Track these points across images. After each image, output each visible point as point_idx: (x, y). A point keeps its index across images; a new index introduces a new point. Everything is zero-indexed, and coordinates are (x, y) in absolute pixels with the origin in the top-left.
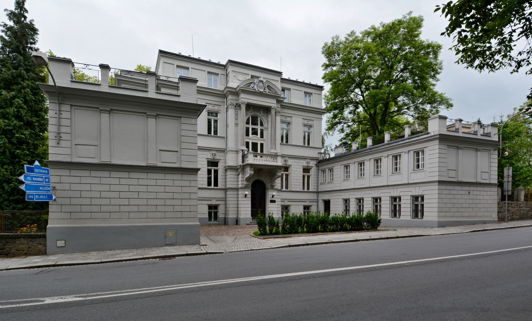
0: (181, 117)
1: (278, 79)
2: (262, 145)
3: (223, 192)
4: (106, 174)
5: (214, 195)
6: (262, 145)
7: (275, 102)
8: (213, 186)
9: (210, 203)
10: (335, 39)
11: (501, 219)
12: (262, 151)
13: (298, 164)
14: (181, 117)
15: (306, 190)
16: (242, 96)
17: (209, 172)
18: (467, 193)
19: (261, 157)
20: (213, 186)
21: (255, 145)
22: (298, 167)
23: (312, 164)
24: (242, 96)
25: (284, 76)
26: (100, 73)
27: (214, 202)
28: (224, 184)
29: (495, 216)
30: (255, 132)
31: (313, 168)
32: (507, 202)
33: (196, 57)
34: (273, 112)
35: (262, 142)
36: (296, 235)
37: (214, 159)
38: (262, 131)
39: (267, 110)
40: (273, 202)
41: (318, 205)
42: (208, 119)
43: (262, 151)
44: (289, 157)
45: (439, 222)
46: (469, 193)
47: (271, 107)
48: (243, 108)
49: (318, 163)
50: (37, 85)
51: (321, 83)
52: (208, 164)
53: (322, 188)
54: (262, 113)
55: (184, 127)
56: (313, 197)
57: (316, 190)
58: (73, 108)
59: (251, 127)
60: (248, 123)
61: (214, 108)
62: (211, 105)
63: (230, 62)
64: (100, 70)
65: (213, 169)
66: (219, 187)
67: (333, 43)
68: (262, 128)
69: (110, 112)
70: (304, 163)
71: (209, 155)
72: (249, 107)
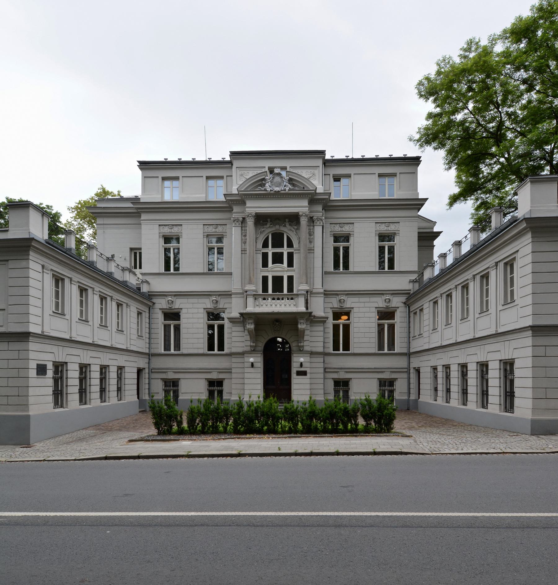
1: (320, 162)
2: (290, 278)
3: (405, 359)
5: (215, 363)
6: (290, 278)
7: (305, 203)
8: (216, 351)
9: (209, 376)
10: (442, 65)
12: (290, 289)
13: (367, 305)
16: (249, 203)
19: (264, 299)
20: (172, 351)
21: (278, 281)
22: (196, 311)
23: (397, 302)
24: (249, 203)
25: (328, 157)
27: (214, 376)
28: (405, 345)
30: (278, 259)
31: (398, 311)
33: (357, 156)
34: (304, 221)
35: (290, 274)
36: (203, 437)
38: (290, 256)
39: (293, 219)
40: (304, 373)
41: (409, 378)
42: (380, 247)
43: (290, 289)
45: (533, 422)
47: (298, 213)
48: (250, 223)
49: (408, 299)
51: (412, 151)
52: (208, 316)
53: (416, 346)
54: (287, 225)
56: (401, 363)
57: (147, 351)
59: (270, 251)
60: (265, 245)
61: (173, 231)
62: (211, 227)
63: (233, 154)
65: (172, 323)
66: (396, 351)
67: (439, 73)
68: (290, 250)
70: (380, 302)
71: (208, 303)
72: (261, 219)
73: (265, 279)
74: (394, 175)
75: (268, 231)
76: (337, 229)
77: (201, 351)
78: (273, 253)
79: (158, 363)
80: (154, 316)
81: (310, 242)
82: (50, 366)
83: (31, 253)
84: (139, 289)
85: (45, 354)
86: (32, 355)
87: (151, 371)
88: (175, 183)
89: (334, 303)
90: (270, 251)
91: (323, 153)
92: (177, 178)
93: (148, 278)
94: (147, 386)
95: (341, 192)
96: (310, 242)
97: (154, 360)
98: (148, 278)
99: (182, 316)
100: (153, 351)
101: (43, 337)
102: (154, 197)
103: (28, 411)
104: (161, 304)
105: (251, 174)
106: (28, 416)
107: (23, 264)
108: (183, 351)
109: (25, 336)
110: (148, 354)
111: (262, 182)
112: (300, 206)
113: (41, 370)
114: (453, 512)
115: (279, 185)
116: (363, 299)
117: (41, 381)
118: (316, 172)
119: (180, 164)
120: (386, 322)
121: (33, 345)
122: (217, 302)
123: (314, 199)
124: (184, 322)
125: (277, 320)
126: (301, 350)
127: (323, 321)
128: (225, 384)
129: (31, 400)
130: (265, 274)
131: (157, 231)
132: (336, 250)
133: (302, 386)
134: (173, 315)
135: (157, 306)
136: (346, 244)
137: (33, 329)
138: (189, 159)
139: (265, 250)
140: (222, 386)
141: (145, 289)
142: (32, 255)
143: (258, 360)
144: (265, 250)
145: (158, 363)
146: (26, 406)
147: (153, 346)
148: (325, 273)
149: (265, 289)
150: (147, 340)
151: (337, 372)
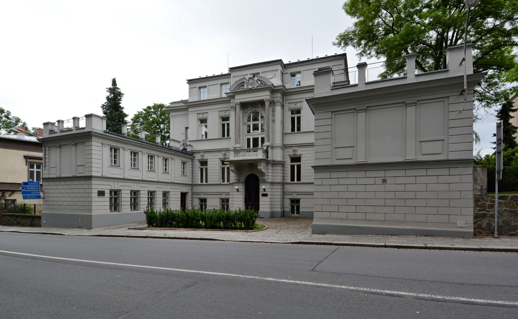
0: (448, 97)
1: (279, 67)
2: (263, 139)
4: (445, 171)
7: (268, 93)
11: (481, 230)
13: (215, 157)
14: (448, 97)
15: (204, 183)
17: (292, 167)
18: (379, 181)
20: (296, 181)
21: (256, 140)
22: (214, 160)
25: (285, 62)
26: (357, 73)
27: (224, 196)
29: (465, 221)
30: (256, 128)
32: (497, 195)
34: (267, 104)
37: (295, 155)
39: (262, 103)
40: (266, 195)
44: (298, 146)
46: (384, 181)
50: (118, 128)
51: (339, 51)
55: (452, 108)
57: (191, 183)
58: (334, 113)
63: (232, 69)
64: (357, 70)
69: (365, 110)
71: (221, 155)
72: (244, 106)
73: (249, 140)
74: (205, 87)
75: (250, 111)
76: (293, 106)
77: (217, 183)
78: (253, 124)
79: (197, 189)
80: (195, 164)
81: (273, 116)
82: (107, 192)
83: (93, 138)
84: (185, 149)
85: (107, 187)
86: (93, 186)
87: (193, 194)
88: (206, 89)
89: (290, 152)
90: (251, 123)
91: (280, 61)
92: (205, 87)
93: (191, 144)
94: (190, 202)
95: (291, 84)
96: (273, 116)
97: (194, 187)
98: (191, 144)
99: (302, 159)
100: (194, 183)
101: (103, 178)
102: (195, 99)
103: (91, 213)
104: (198, 157)
105: (238, 79)
106: (91, 216)
107: (90, 143)
108: (209, 183)
109: (90, 178)
110: (191, 185)
111: (242, 84)
112: (265, 96)
113: (101, 193)
114: (192, 273)
115: (252, 84)
116: (308, 149)
117: (101, 199)
118: (277, 73)
119: (207, 79)
120: (296, 164)
121: (94, 182)
122: (225, 154)
123: (273, 90)
124: (209, 166)
125: (250, 164)
126: (265, 182)
127: (282, 164)
128: (230, 200)
129: (93, 208)
130: (249, 137)
131: (196, 117)
132: (293, 119)
133: (265, 203)
134: (204, 163)
135: (196, 158)
136: (298, 115)
137: (94, 174)
138: (296, 61)
139: (249, 123)
140: (299, 203)
141: (189, 149)
142: (94, 139)
143: (241, 187)
144: (249, 123)
145: (197, 189)
146: (90, 210)
147: (194, 180)
148: (284, 134)
149: (249, 146)
150: (191, 177)
151: (291, 194)
